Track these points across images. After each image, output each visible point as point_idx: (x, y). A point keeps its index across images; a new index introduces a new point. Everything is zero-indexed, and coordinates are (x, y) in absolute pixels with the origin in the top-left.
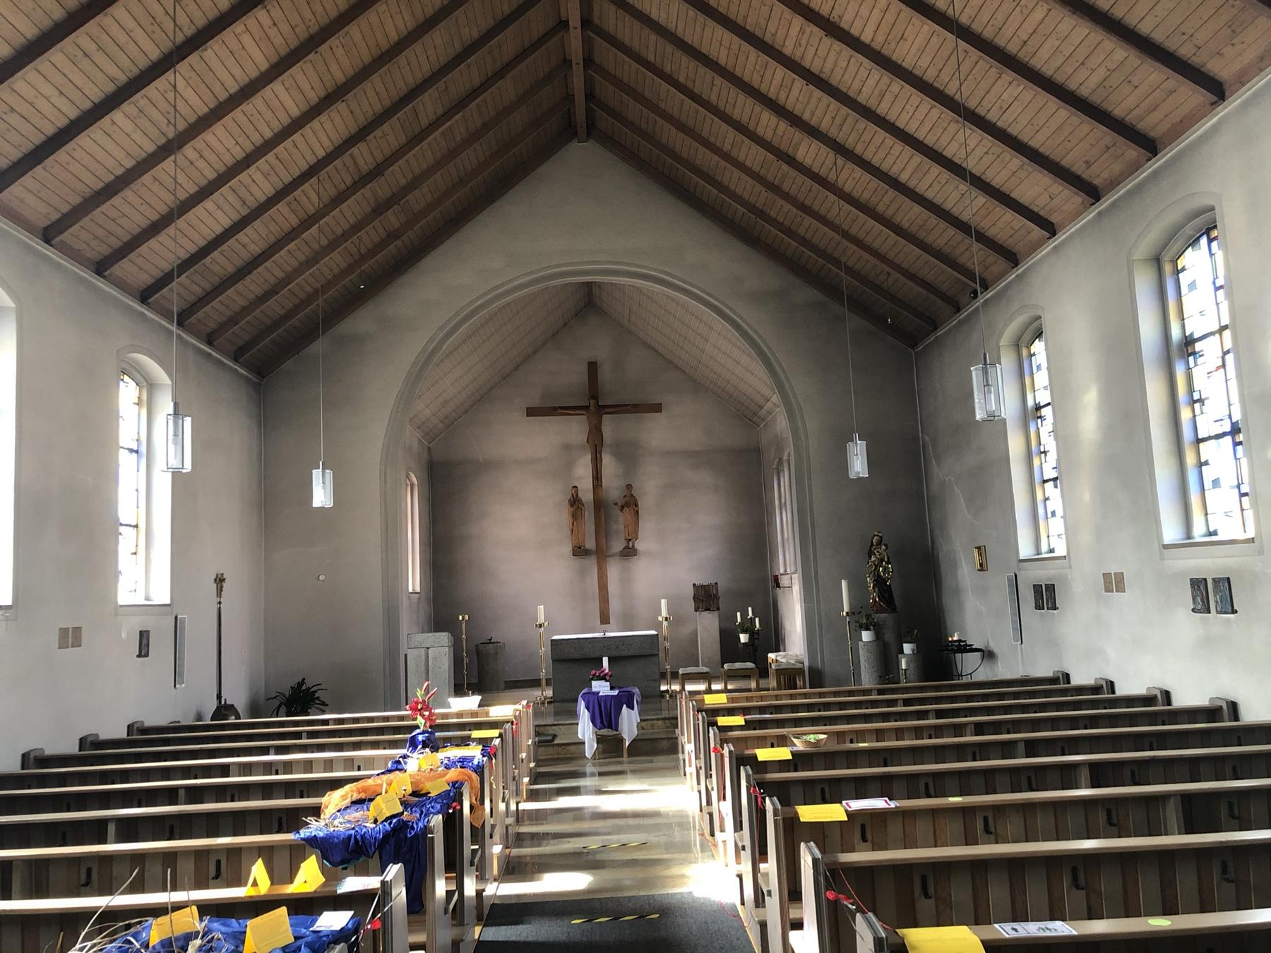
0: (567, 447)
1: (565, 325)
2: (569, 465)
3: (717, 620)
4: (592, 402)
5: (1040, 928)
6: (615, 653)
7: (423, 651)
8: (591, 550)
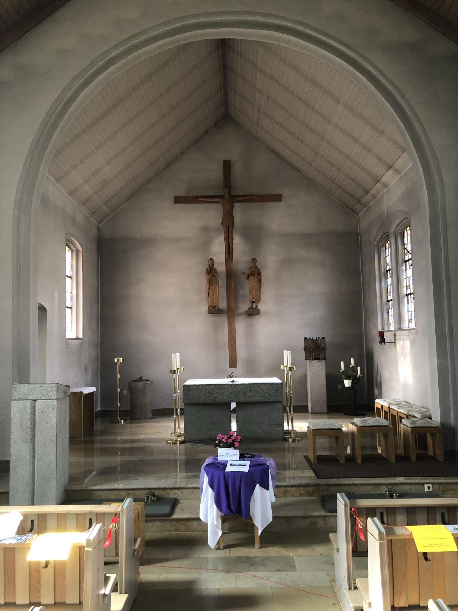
0: (206, 229)
1: (207, 132)
2: (208, 243)
3: (324, 366)
4: (226, 190)
5: (455, 528)
6: (242, 399)
7: (28, 404)
8: (223, 310)
